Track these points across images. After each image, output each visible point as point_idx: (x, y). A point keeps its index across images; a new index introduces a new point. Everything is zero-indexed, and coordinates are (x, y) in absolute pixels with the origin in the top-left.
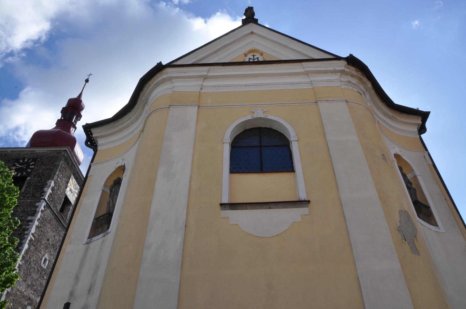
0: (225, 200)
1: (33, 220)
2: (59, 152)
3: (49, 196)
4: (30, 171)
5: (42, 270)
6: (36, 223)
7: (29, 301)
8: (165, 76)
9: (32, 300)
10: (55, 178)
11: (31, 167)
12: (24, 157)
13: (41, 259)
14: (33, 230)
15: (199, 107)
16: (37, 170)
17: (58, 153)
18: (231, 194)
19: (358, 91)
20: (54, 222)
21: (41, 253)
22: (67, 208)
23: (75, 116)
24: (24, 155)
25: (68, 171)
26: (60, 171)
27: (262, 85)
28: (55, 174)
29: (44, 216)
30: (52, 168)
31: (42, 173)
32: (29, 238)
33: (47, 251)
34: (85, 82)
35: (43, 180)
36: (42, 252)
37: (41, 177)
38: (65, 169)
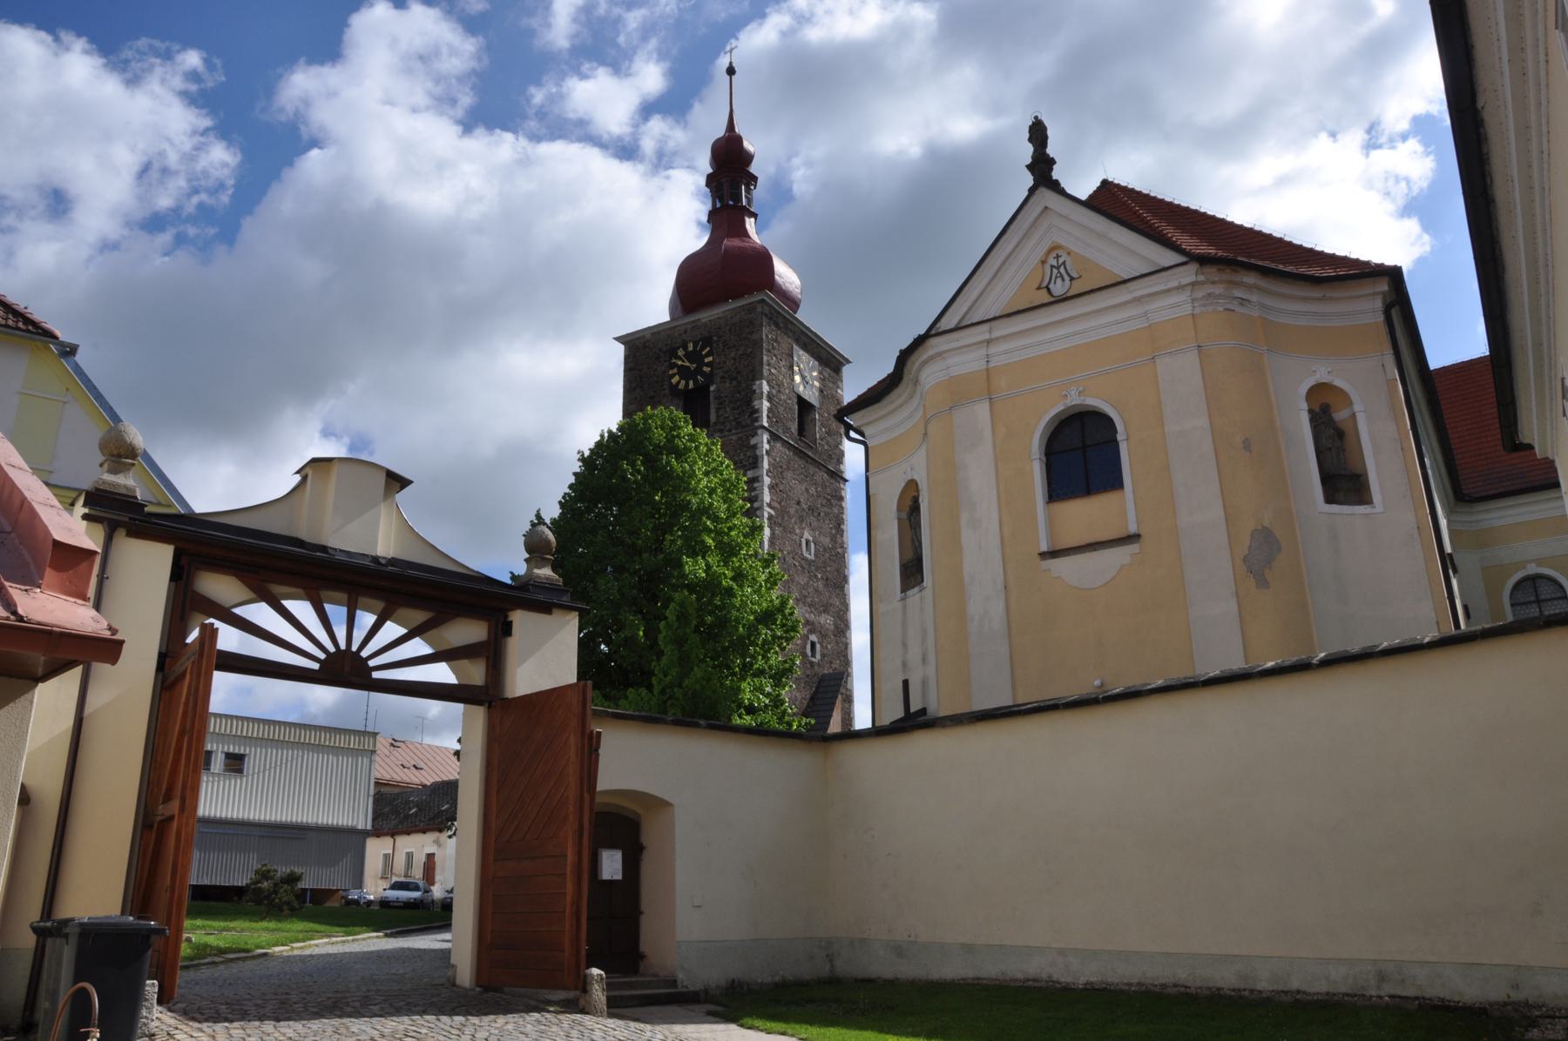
0: (1044, 548)
1: (758, 477)
2: (751, 308)
3: (768, 417)
4: (709, 369)
5: (810, 565)
6: (767, 480)
7: (809, 627)
8: (931, 352)
9: (813, 624)
10: (765, 373)
11: (706, 360)
12: (684, 340)
13: (800, 545)
14: (767, 498)
15: (991, 399)
16: (721, 365)
17: (749, 310)
18: (1051, 535)
19: (1226, 309)
20: (798, 463)
21: (796, 535)
22: (810, 419)
23: (743, 187)
24: (680, 335)
25: (786, 341)
26: (769, 351)
27: (1075, 334)
28: (762, 364)
29: (775, 460)
30: (749, 351)
31: (736, 369)
32: (766, 515)
33: (804, 525)
34: (728, 77)
35: (744, 385)
36: (797, 531)
37: (735, 379)
38: (776, 341)
